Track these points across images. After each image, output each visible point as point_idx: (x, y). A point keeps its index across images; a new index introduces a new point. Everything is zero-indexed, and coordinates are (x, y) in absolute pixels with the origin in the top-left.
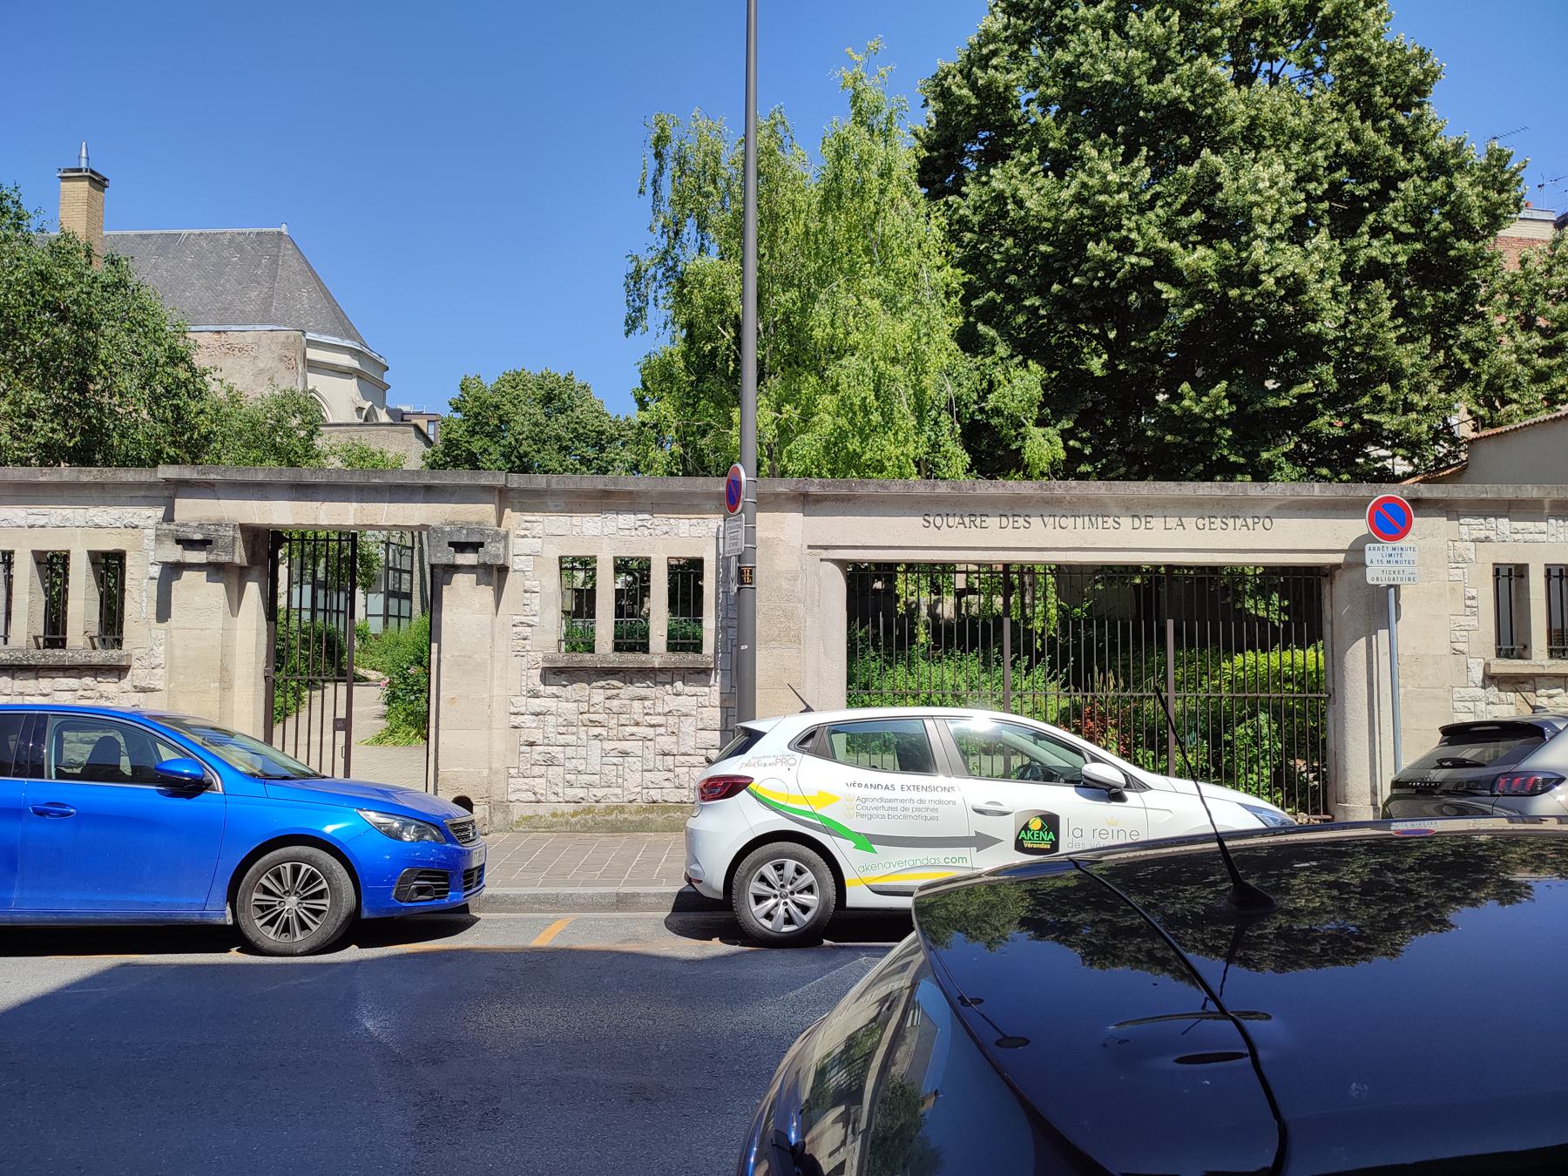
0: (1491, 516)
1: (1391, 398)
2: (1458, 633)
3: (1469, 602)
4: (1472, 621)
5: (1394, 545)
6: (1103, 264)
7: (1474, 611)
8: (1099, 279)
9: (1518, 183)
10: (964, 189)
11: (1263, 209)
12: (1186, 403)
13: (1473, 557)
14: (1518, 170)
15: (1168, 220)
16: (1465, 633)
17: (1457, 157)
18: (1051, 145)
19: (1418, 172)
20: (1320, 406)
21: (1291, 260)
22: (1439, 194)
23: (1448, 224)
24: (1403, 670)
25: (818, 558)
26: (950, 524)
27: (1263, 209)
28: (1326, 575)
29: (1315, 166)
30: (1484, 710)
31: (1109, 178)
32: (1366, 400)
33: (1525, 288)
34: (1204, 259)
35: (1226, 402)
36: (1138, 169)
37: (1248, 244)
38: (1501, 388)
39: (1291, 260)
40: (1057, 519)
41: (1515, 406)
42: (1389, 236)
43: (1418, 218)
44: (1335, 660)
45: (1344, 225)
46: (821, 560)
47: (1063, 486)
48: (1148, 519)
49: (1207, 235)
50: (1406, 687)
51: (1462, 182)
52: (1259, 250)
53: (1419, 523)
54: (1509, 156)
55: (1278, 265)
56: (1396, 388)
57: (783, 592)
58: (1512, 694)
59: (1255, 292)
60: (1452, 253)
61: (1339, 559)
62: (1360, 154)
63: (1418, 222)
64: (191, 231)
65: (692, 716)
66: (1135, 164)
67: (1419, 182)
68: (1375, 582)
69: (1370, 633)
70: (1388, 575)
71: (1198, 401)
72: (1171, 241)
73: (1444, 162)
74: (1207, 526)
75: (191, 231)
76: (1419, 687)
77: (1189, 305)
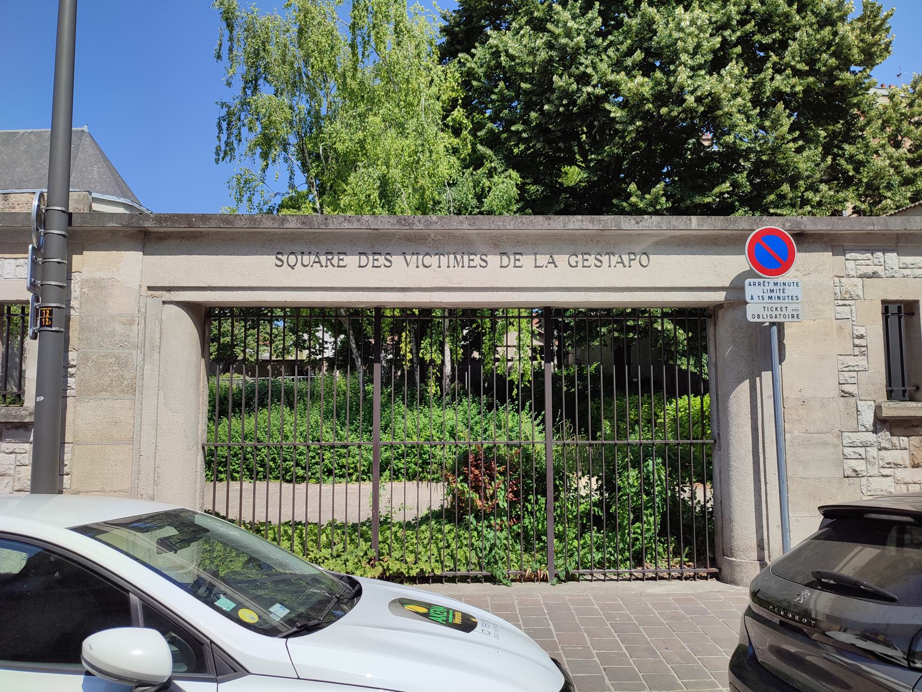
0: (879, 251)
1: (790, 195)
2: (846, 374)
3: (857, 342)
4: (862, 362)
5: (776, 281)
6: (566, 93)
7: (863, 350)
8: (564, 106)
9: (887, 30)
10: (473, 50)
11: (685, 42)
12: (633, 199)
13: (861, 293)
14: (887, 17)
15: (617, 60)
16: (854, 374)
17: (840, 11)
18: (536, 14)
19: (811, 25)
20: (737, 203)
21: (708, 83)
22: (827, 39)
23: (834, 59)
24: (790, 413)
25: (160, 300)
26: (305, 263)
27: (685, 42)
28: (710, 316)
29: (730, 18)
30: (876, 456)
31: (569, 24)
32: (772, 197)
33: (894, 115)
34: (642, 85)
35: (664, 199)
36: (593, 19)
37: (675, 71)
38: (878, 188)
39: (708, 83)
40: (420, 257)
41: (889, 201)
42: (789, 71)
43: (811, 59)
44: (720, 404)
45: (755, 65)
46: (164, 303)
47: (423, 220)
48: (518, 257)
49: (646, 69)
50: (793, 433)
51: (842, 28)
52: (683, 75)
53: (802, 259)
54: (879, 8)
55: (699, 86)
56: (794, 187)
57: (117, 338)
58: (905, 439)
59: (680, 109)
60: (837, 83)
61: (720, 297)
62: (765, 13)
63: (811, 62)
64: (25, 130)
65: (9, 475)
66: (590, 15)
67: (811, 32)
68: (756, 320)
69: (753, 376)
70: (770, 312)
71: (642, 198)
72: (618, 73)
73: (830, 17)
74: (580, 264)
75: (25, 130)
76: (807, 432)
77: (632, 122)
